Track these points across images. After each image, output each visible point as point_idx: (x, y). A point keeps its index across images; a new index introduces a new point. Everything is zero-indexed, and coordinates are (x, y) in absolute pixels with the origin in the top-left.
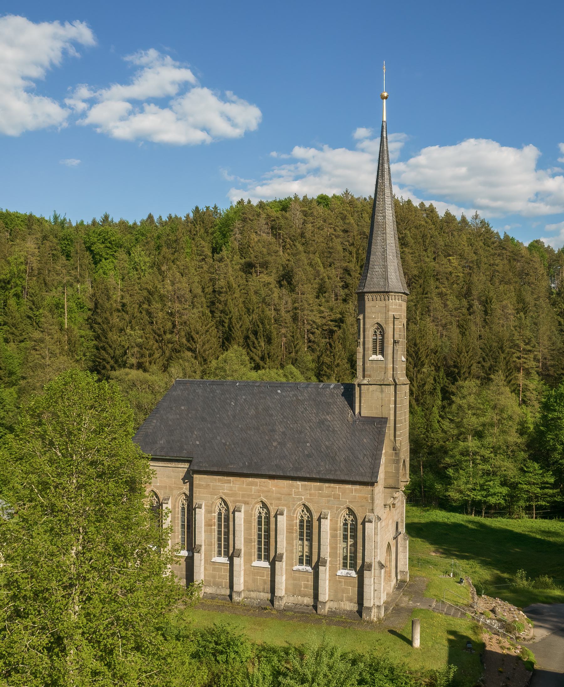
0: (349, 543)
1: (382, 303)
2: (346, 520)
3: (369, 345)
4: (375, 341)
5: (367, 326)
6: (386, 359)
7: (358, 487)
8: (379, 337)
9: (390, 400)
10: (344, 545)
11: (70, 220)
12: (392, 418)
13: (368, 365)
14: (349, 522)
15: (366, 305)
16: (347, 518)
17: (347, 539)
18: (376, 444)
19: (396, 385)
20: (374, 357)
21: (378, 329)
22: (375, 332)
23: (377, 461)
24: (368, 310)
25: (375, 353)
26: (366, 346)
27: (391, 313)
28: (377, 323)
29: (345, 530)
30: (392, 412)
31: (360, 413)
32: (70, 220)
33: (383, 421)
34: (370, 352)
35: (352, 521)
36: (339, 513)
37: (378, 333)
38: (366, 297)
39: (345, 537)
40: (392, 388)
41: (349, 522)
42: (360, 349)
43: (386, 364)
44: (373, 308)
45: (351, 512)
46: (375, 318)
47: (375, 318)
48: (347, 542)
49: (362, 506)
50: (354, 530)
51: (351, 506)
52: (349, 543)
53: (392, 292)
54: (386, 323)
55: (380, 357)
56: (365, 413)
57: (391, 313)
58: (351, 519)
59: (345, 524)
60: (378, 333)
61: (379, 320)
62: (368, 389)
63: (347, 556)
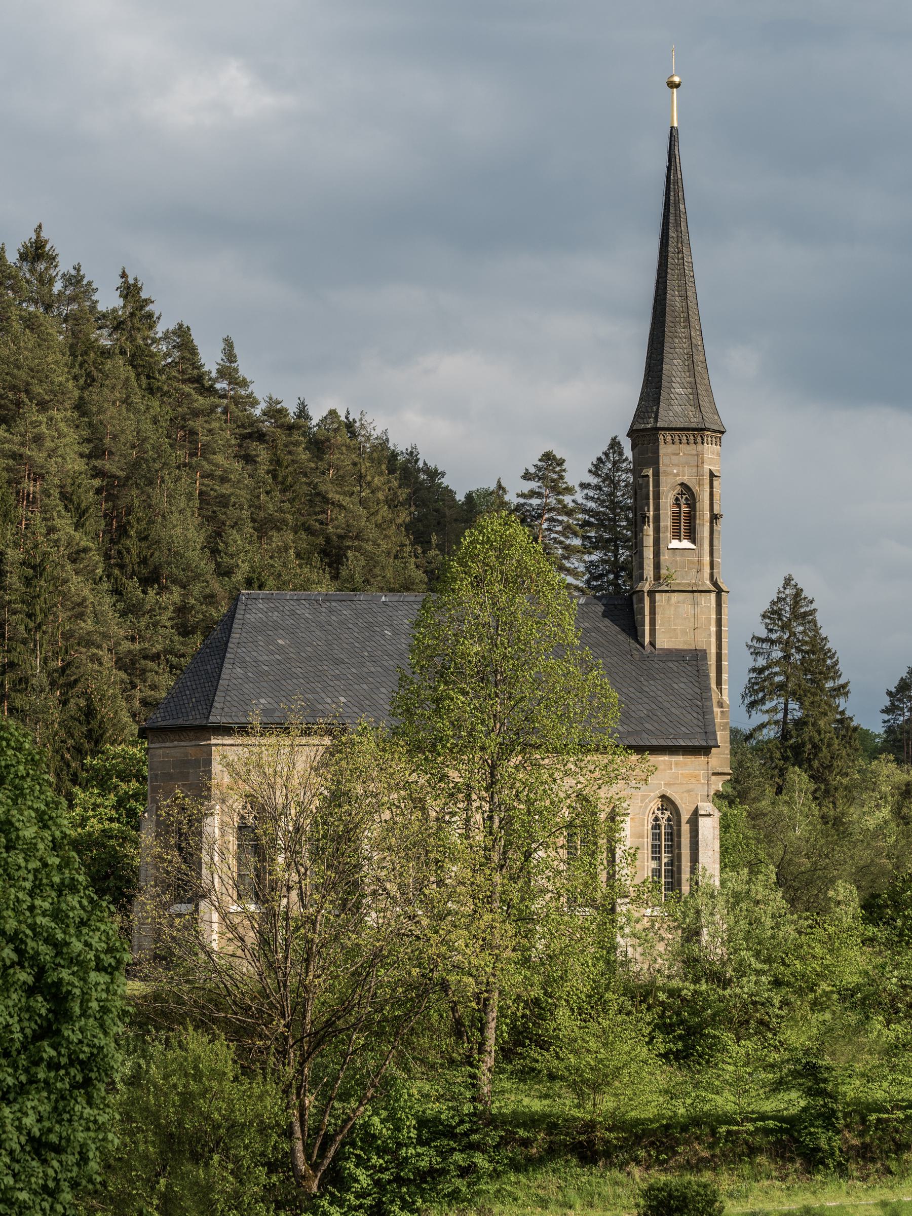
0: (664, 860)
1: (691, 449)
2: (656, 819)
3: (667, 522)
4: (676, 516)
5: (663, 488)
6: (701, 547)
7: (680, 758)
8: (684, 509)
9: (709, 619)
10: (653, 865)
11: (130, 291)
12: (713, 650)
13: (665, 558)
14: (663, 823)
15: (661, 452)
16: (660, 816)
17: (660, 852)
18: (699, 691)
19: (719, 592)
20: (675, 544)
21: (682, 494)
22: (677, 499)
23: (709, 703)
24: (663, 460)
25: (677, 536)
26: (662, 524)
27: (707, 467)
28: (682, 484)
29: (656, 837)
30: (713, 639)
31: (652, 644)
32: (130, 291)
33: (697, 657)
34: (669, 535)
35: (669, 820)
36: (646, 807)
37: (683, 501)
38: (661, 437)
39: (656, 849)
40: (713, 596)
41: (663, 823)
42: (649, 530)
43: (700, 556)
44: (673, 457)
45: (667, 802)
46: (677, 475)
47: (677, 475)
48: (659, 859)
49: (689, 791)
50: (674, 836)
51: (669, 793)
52: (664, 860)
53: (708, 430)
54: (700, 483)
55: (686, 544)
56: (664, 641)
57: (707, 467)
58: (666, 817)
59: (656, 826)
60: (683, 501)
61: (685, 479)
62: (669, 600)
63: (660, 871)
